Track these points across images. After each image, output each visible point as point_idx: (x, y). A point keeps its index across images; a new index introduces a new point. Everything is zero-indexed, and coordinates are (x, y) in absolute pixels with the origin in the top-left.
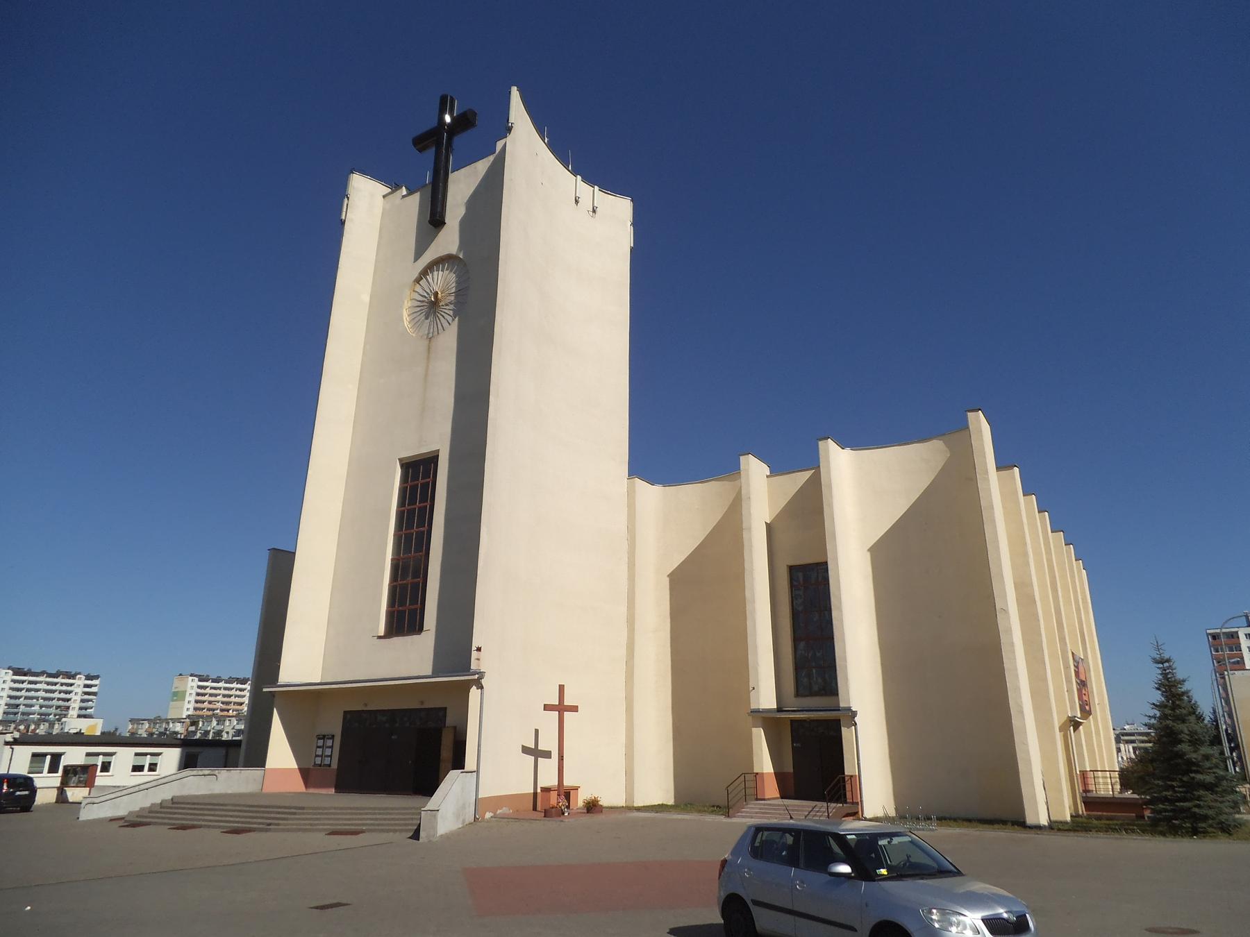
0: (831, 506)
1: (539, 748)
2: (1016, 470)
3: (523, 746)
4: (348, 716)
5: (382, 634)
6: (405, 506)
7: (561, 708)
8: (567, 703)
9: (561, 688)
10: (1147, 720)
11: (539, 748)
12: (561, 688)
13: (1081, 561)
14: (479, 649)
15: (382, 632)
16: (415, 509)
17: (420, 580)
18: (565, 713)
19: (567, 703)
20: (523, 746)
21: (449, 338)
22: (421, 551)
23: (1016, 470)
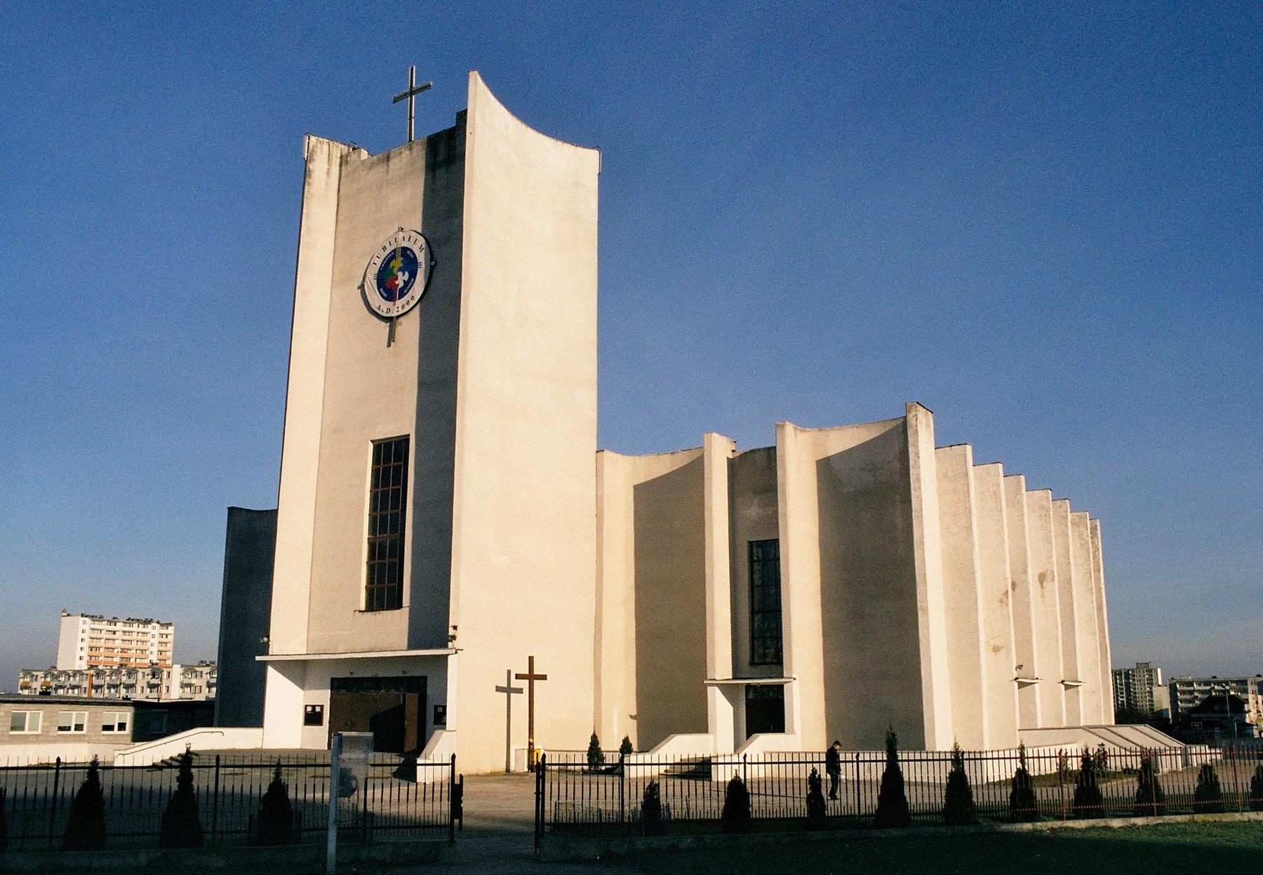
0: (785, 500)
1: (512, 687)
2: (969, 448)
3: (497, 687)
4: (336, 683)
5: (364, 609)
6: (375, 560)
7: (531, 677)
8: (536, 673)
9: (531, 659)
10: (1153, 748)
11: (512, 687)
12: (531, 659)
13: (1000, 465)
14: (455, 628)
15: (363, 606)
16: (389, 490)
17: (397, 560)
18: (535, 681)
19: (536, 673)
20: (497, 687)
21: (410, 329)
22: (398, 508)
23: (969, 448)
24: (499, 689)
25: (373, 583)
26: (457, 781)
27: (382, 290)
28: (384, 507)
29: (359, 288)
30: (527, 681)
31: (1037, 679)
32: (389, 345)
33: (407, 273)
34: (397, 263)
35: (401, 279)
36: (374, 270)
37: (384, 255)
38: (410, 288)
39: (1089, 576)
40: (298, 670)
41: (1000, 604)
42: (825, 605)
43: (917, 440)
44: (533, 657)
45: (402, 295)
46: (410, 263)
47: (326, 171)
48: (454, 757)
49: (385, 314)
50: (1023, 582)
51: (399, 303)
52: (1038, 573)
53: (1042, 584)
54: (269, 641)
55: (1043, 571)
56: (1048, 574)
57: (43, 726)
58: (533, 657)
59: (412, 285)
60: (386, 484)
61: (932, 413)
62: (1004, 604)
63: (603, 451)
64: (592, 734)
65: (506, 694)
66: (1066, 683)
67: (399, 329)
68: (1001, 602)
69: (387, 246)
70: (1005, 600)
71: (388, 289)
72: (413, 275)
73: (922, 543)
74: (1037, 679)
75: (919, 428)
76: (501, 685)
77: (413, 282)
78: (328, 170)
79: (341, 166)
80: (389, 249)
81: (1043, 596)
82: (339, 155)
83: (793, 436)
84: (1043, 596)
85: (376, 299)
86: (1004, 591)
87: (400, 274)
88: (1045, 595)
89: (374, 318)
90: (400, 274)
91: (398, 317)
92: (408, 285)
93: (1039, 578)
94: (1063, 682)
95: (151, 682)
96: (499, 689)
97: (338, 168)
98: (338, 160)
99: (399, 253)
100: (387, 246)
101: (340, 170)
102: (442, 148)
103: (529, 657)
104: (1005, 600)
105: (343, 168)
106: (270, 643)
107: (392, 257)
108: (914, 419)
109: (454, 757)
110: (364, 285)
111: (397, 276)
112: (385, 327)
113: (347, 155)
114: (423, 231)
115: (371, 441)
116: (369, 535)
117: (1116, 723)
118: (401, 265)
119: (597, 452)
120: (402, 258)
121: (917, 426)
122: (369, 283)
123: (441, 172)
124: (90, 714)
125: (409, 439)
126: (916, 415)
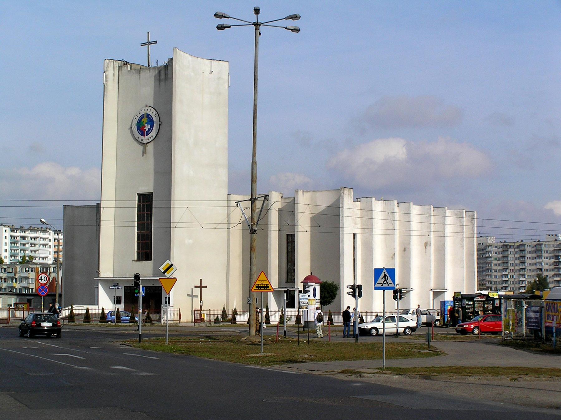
3: (188, 294)
5: (136, 260)
7: (201, 287)
9: (201, 280)
12: (201, 280)
15: (136, 259)
24: (188, 295)
25: (140, 250)
26: (180, 313)
27: (139, 130)
28: (143, 220)
29: (129, 129)
30: (199, 288)
31: (412, 289)
32: (143, 156)
33: (149, 125)
34: (145, 120)
35: (147, 127)
36: (135, 122)
37: (139, 115)
38: (151, 132)
39: (462, 240)
40: (111, 284)
41: (391, 259)
42: (312, 260)
43: (343, 201)
44: (201, 279)
45: (147, 135)
46: (151, 122)
47: (113, 74)
48: (179, 309)
49: (140, 141)
50: (409, 248)
51: (147, 137)
52: (424, 243)
53: (426, 247)
54: (99, 272)
55: (426, 241)
56: (428, 243)
57: (34, 305)
58: (201, 279)
59: (152, 131)
60: (143, 211)
61: (352, 189)
62: (393, 259)
63: (230, 194)
64: (223, 308)
65: (191, 298)
66: (432, 290)
67: (147, 148)
68: (392, 258)
69: (141, 112)
70: (393, 257)
71: (143, 133)
72: (152, 126)
73: (343, 240)
74: (412, 289)
75: (344, 197)
76: (189, 294)
77: (152, 130)
78: (114, 73)
79: (119, 71)
80: (142, 114)
81: (426, 252)
82: (118, 66)
83: (302, 195)
84: (426, 252)
85: (137, 135)
86: (393, 253)
87: (146, 125)
88: (427, 252)
89: (136, 143)
90: (146, 125)
91: (147, 143)
92: (150, 130)
93: (425, 244)
94: (431, 290)
95: (458, 329)
96: (188, 295)
97: (118, 72)
98: (118, 68)
99: (145, 116)
100: (141, 112)
101: (119, 73)
102: (163, 72)
103: (200, 279)
104: (393, 257)
105: (120, 72)
106: (100, 273)
107: (142, 117)
108: (343, 193)
109: (179, 309)
110: (131, 127)
111: (145, 126)
112: (141, 148)
113: (121, 66)
114: (155, 103)
115: (137, 193)
116: (137, 230)
117: (31, 299)
118: (147, 121)
119: (228, 195)
120: (147, 119)
121: (343, 196)
122: (134, 127)
123: (162, 83)
124: (2, 299)
125: (152, 194)
126: (343, 192)
